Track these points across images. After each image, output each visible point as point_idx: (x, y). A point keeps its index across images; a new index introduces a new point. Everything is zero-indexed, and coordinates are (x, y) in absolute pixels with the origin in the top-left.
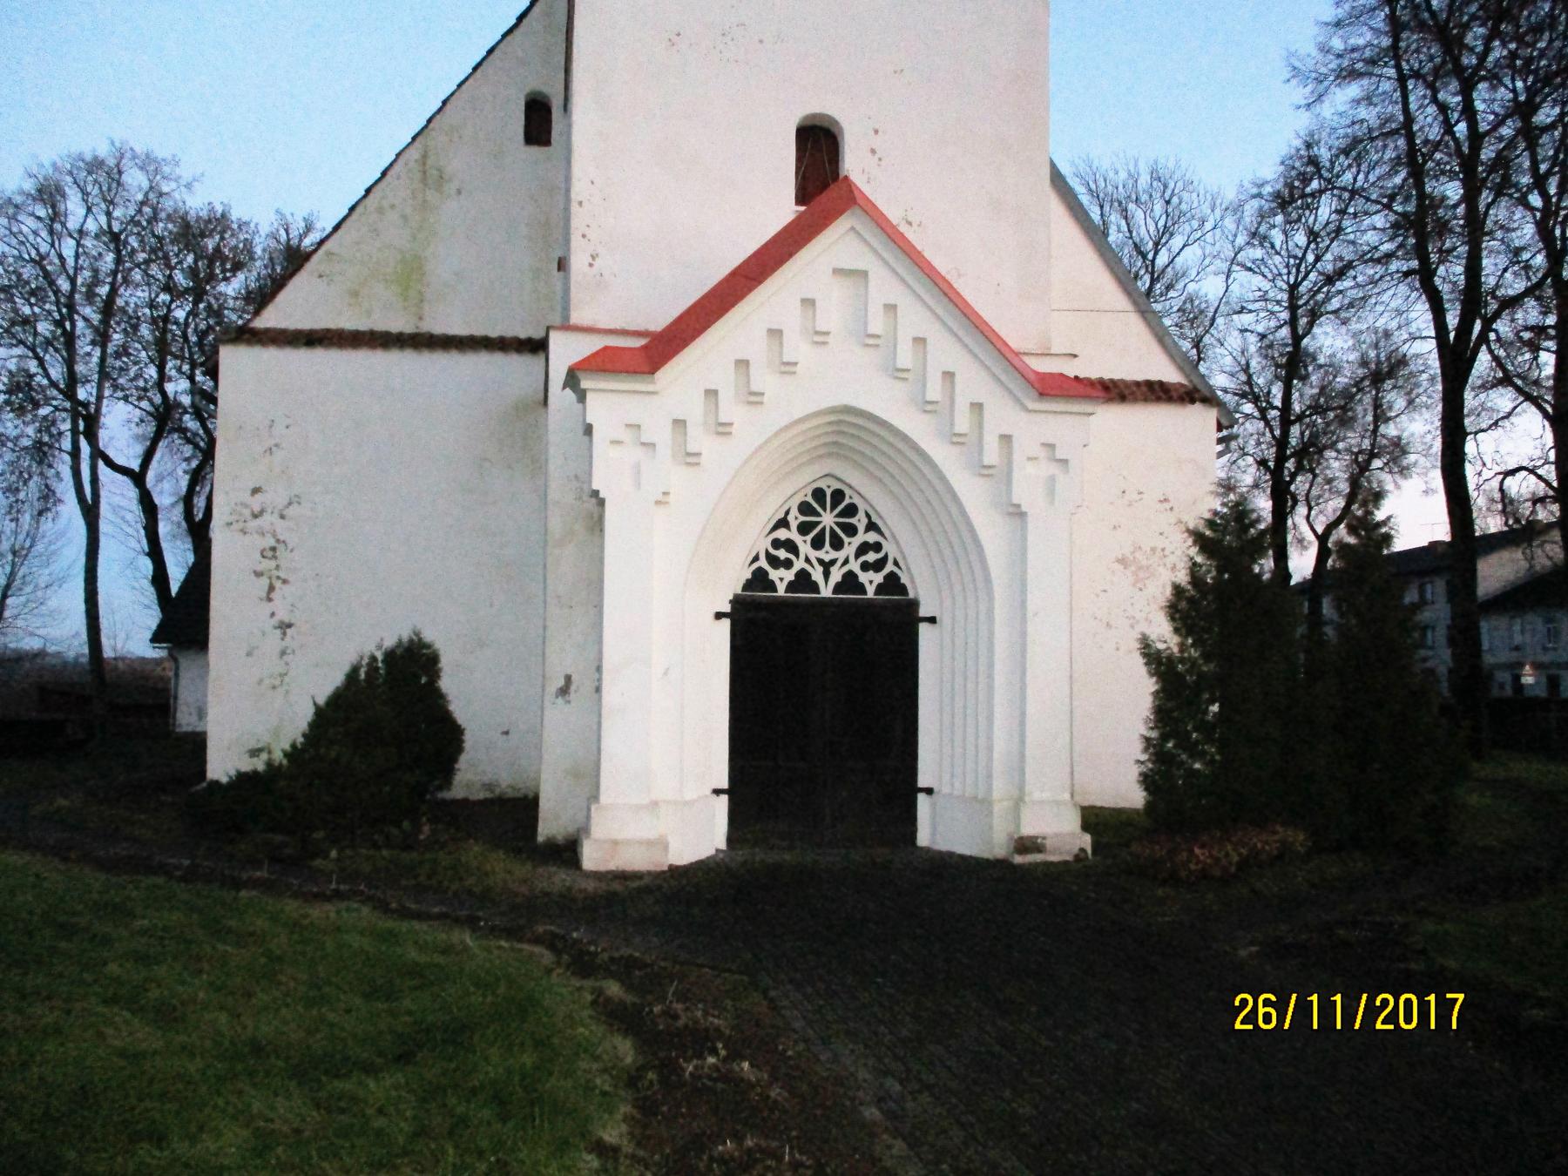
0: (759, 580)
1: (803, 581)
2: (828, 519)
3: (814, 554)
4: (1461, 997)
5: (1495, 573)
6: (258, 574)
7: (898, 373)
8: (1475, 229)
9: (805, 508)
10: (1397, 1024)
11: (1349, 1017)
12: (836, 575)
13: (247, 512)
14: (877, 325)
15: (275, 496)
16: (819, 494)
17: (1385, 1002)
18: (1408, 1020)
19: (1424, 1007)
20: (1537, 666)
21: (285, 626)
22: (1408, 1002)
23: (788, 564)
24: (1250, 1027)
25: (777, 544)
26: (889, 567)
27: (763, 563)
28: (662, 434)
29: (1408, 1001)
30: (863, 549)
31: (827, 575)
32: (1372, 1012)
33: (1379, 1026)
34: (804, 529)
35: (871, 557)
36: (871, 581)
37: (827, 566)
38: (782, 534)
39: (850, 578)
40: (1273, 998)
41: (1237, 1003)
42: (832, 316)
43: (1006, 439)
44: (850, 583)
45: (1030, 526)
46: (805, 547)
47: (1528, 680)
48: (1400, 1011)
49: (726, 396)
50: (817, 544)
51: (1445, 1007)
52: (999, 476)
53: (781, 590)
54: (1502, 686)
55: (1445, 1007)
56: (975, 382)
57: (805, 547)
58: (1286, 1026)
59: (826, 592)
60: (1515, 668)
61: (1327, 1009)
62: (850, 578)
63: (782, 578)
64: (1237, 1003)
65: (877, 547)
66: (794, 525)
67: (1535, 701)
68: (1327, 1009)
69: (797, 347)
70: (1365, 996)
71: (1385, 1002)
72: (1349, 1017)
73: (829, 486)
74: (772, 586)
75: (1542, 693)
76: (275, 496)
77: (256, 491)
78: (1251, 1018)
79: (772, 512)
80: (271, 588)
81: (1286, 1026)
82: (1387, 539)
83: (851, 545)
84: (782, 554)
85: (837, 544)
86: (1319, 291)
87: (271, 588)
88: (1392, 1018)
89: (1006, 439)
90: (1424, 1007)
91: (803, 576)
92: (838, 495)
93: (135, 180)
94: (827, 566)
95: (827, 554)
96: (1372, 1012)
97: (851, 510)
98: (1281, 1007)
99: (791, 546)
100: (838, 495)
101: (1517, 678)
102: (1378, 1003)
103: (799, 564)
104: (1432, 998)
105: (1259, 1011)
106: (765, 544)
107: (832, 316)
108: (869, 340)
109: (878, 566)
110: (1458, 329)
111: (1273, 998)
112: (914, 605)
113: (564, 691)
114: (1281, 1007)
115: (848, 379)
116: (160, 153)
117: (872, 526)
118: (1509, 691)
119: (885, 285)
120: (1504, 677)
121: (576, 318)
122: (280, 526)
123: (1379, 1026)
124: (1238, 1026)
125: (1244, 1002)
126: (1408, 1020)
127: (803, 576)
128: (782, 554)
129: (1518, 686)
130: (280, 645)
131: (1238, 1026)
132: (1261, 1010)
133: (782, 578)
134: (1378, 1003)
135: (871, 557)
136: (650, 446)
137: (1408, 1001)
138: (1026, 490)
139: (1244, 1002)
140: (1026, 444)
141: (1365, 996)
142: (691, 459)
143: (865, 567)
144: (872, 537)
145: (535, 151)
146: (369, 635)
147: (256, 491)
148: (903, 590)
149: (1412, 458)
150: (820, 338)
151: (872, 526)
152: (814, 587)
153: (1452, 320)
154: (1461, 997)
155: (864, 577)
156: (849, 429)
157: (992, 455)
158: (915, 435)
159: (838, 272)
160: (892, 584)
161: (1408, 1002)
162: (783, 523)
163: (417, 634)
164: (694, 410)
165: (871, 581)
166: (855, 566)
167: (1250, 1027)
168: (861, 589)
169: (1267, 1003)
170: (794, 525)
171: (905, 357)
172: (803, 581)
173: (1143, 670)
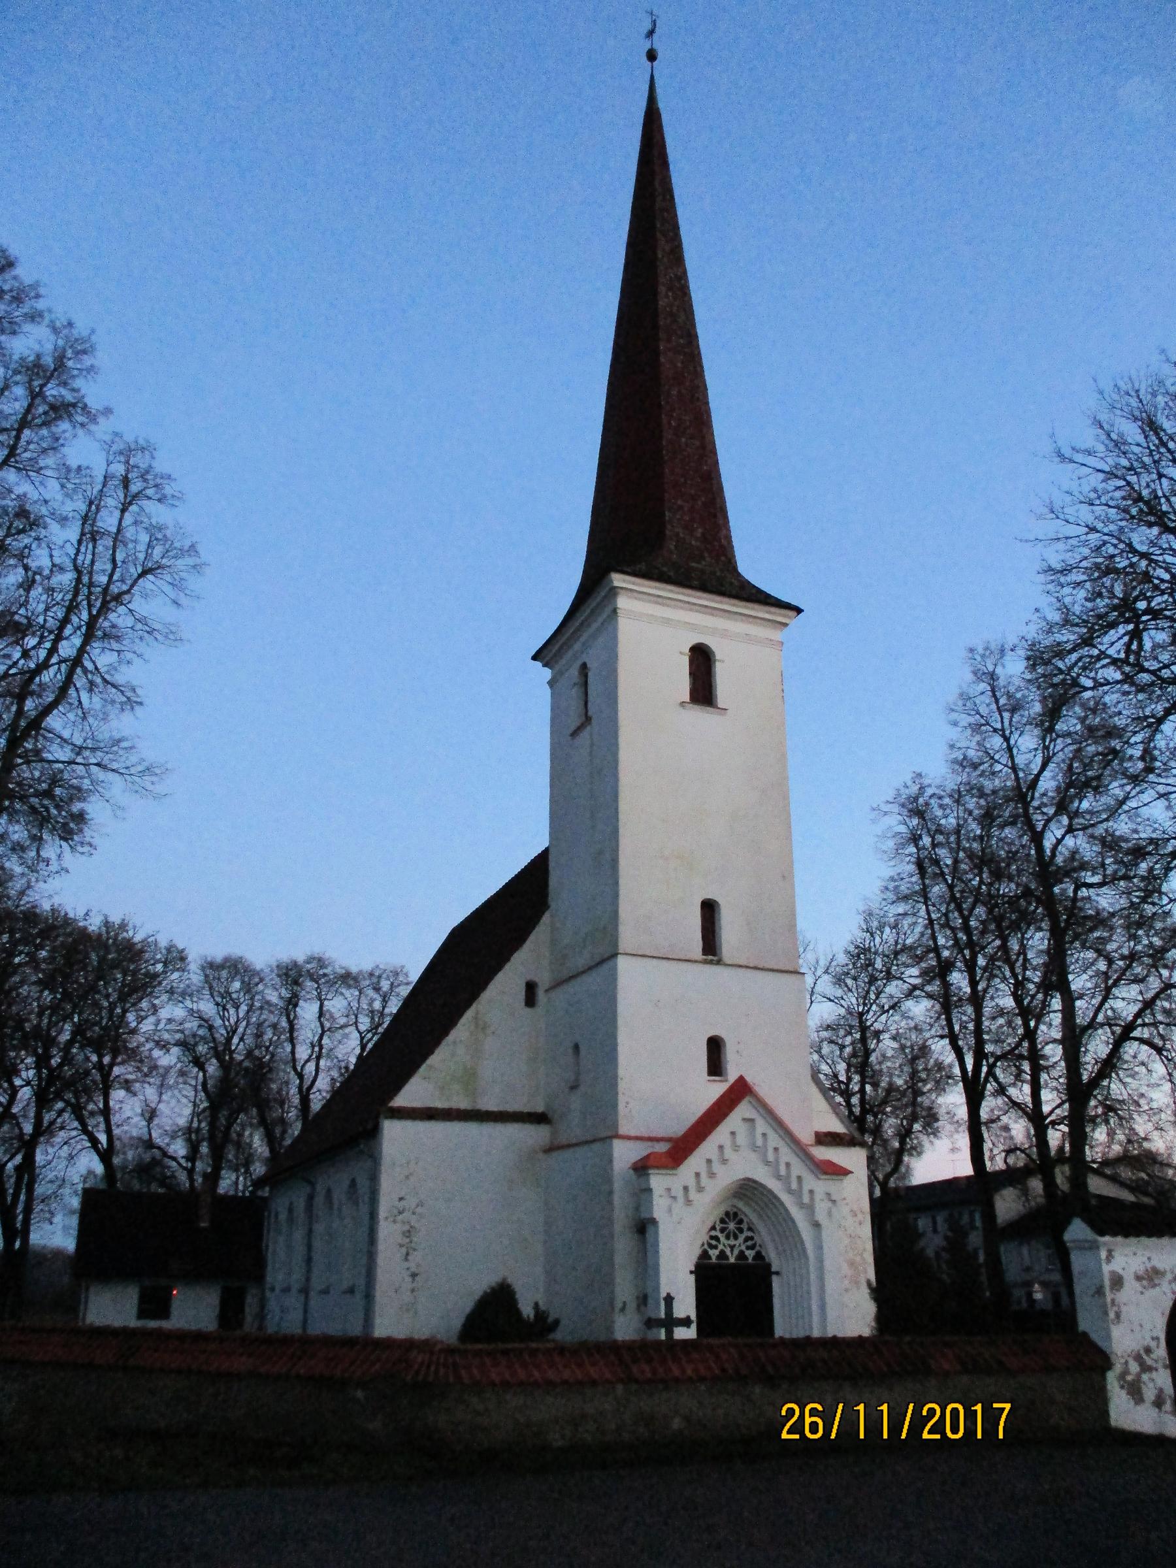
0: (704, 1255)
1: (722, 1255)
2: (732, 1226)
3: (726, 1242)
4: (1008, 1406)
5: (1007, 1205)
6: (401, 1246)
7: (767, 1163)
8: (977, 1000)
9: (722, 1221)
10: (943, 1434)
12: (736, 1252)
13: (396, 1212)
15: (411, 1202)
16: (727, 1214)
17: (932, 1412)
18: (955, 1430)
19: (971, 1416)
20: (1045, 1285)
21: (414, 1275)
22: (955, 1412)
23: (716, 1247)
24: (797, 1437)
25: (712, 1238)
26: (758, 1248)
27: (706, 1246)
28: (680, 1194)
30: (747, 1239)
31: (732, 1251)
34: (722, 1230)
35: (749, 1243)
36: (750, 1254)
38: (713, 1233)
39: (742, 1252)
40: (820, 1408)
42: (742, 1139)
43: (811, 1192)
45: (824, 1234)
46: (722, 1239)
47: (1038, 1296)
49: (704, 1175)
50: (728, 1238)
51: (991, 1417)
52: (810, 1208)
53: (714, 1260)
54: (1019, 1303)
55: (991, 1417)
57: (722, 1239)
59: (732, 1260)
60: (1028, 1284)
62: (742, 1252)
63: (714, 1253)
65: (752, 1238)
66: (718, 1228)
67: (1043, 1313)
69: (728, 1153)
71: (932, 1412)
73: (732, 1210)
74: (710, 1258)
75: (1049, 1306)
76: (411, 1202)
77: (401, 1199)
78: (798, 1428)
79: (710, 1225)
80: (407, 1254)
83: (742, 1237)
84: (714, 1242)
85: (736, 1238)
86: (868, 992)
87: (407, 1254)
88: (939, 1428)
89: (811, 1192)
90: (971, 1416)
91: (722, 1253)
92: (735, 1214)
94: (732, 1247)
95: (732, 1242)
99: (716, 1238)
100: (735, 1214)
101: (1029, 1295)
103: (721, 1247)
104: (979, 1407)
106: (706, 1238)
107: (742, 1139)
108: (754, 1148)
110: (973, 1070)
111: (820, 1408)
112: (769, 1265)
113: (623, 1309)
115: (746, 1165)
117: (750, 1229)
118: (1025, 1305)
119: (761, 1126)
120: (1018, 1293)
121: (622, 1130)
122: (414, 1220)
125: (791, 1412)
126: (955, 1430)
127: (722, 1253)
128: (714, 1242)
129: (1031, 1302)
130: (410, 1286)
133: (714, 1253)
135: (749, 1243)
136: (674, 1198)
138: (821, 1216)
139: (791, 1412)
140: (819, 1196)
142: (688, 1202)
143: (748, 1248)
144: (750, 1234)
145: (528, 1010)
146: (480, 1283)
147: (401, 1199)
148: (763, 1258)
149: (940, 1123)
150: (736, 1148)
152: (727, 1258)
153: (970, 1067)
154: (1008, 1406)
155: (747, 1253)
156: (748, 1190)
157: (806, 1199)
158: (776, 1191)
159: (744, 1119)
160: (759, 1256)
161: (955, 1412)
162: (713, 1228)
163: (504, 1279)
164: (691, 1183)
165: (750, 1254)
166: (743, 1248)
167: (797, 1437)
168: (746, 1258)
169: (814, 1412)
170: (718, 1228)
171: (771, 1157)
172: (722, 1255)
173: (867, 1296)
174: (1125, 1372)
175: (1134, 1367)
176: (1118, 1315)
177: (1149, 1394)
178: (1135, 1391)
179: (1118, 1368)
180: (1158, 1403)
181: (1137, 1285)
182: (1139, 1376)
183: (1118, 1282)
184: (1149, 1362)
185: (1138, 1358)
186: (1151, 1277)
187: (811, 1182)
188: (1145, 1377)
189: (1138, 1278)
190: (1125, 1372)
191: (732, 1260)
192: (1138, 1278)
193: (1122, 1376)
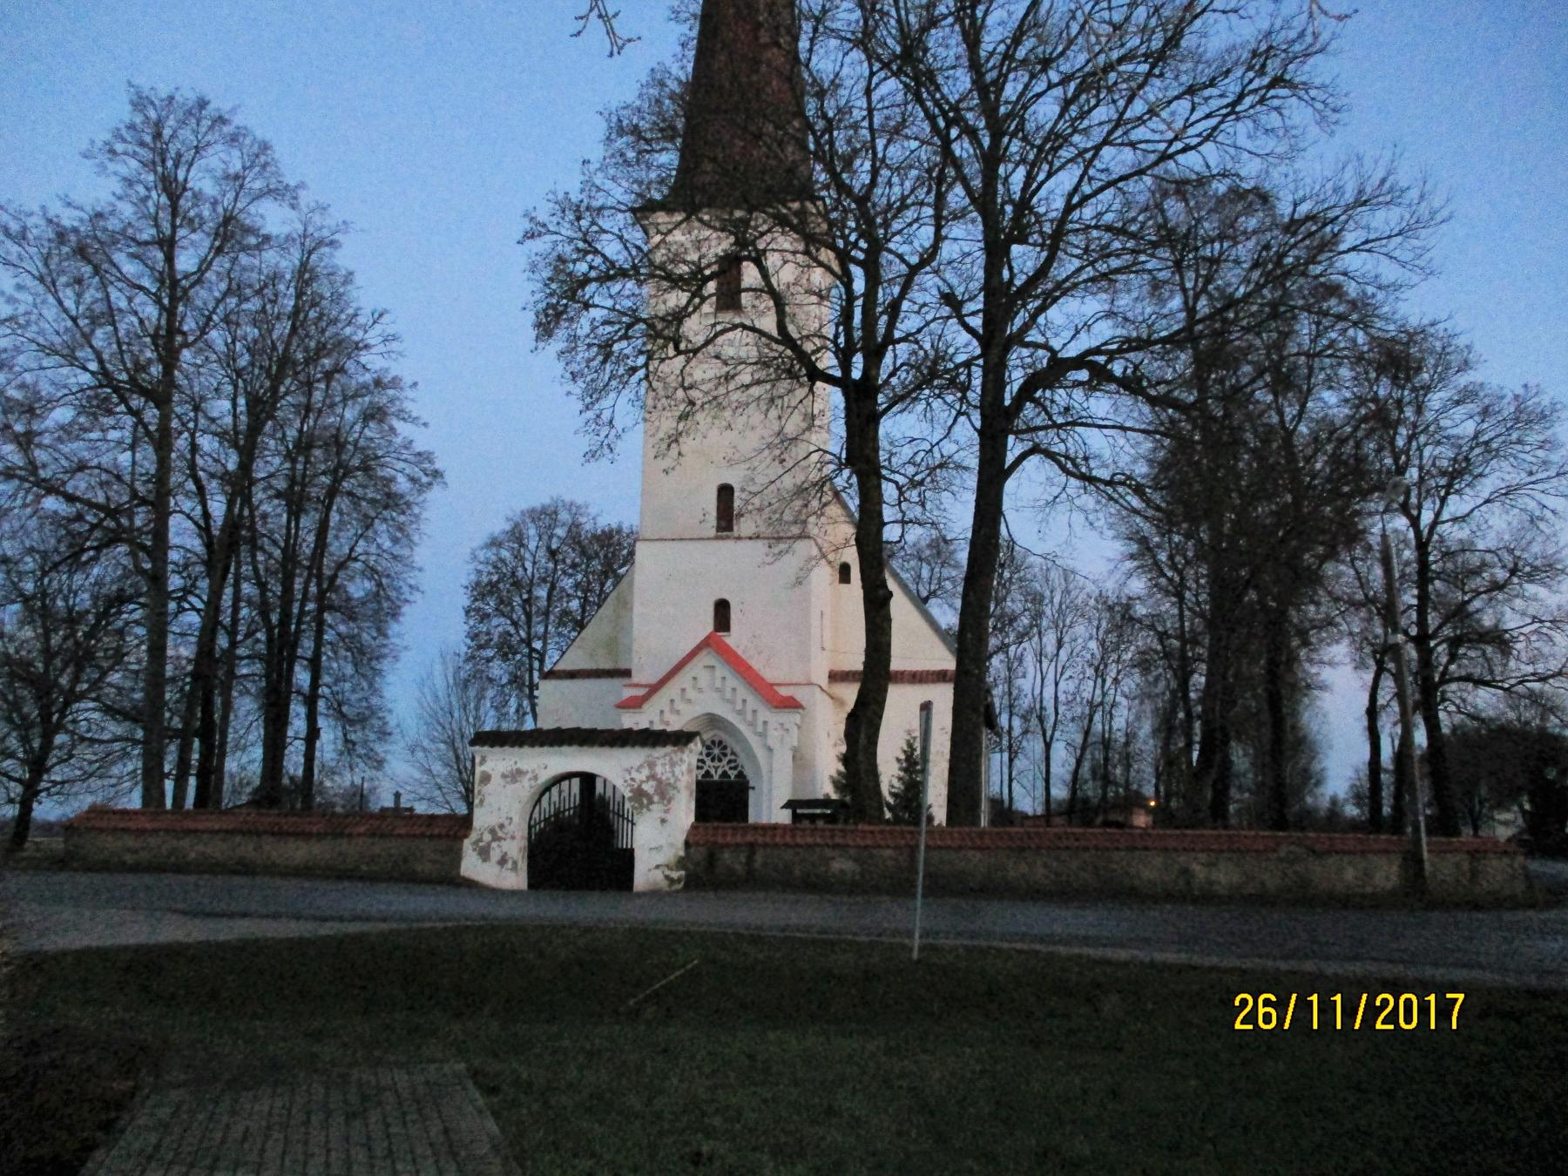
4: (1461, 997)
10: (1397, 1023)
11: (1350, 1013)
12: (720, 771)
14: (718, 684)
17: (1385, 1002)
18: (1408, 1020)
19: (1424, 1009)
22: (1408, 1003)
24: (1250, 1027)
29: (1408, 1001)
32: (1373, 1011)
33: (1379, 1026)
34: (708, 755)
36: (733, 774)
37: (716, 768)
40: (1273, 998)
41: (1237, 1003)
43: (765, 723)
44: (725, 774)
48: (1401, 1012)
51: (1445, 1009)
55: (1445, 1009)
56: (753, 702)
57: (708, 762)
58: (1286, 1026)
59: (716, 778)
61: (1327, 1009)
64: (1237, 1003)
68: (1327, 1009)
70: (1365, 996)
71: (1385, 1002)
72: (1350, 1013)
78: (1251, 1018)
81: (1286, 1026)
82: (839, 773)
88: (1392, 1018)
89: (765, 723)
90: (1424, 1009)
93: (564, 516)
94: (716, 768)
95: (716, 763)
96: (1373, 1011)
97: (725, 748)
98: (1281, 1006)
102: (1378, 1003)
104: (1432, 998)
105: (1259, 1011)
109: (735, 768)
111: (1273, 998)
114: (1281, 1006)
116: (579, 501)
119: (722, 670)
123: (1379, 1026)
124: (1238, 1026)
125: (1244, 1002)
126: (1408, 1020)
131: (1238, 1026)
132: (1261, 1010)
134: (1378, 1003)
137: (1408, 1001)
139: (1244, 1002)
141: (1365, 996)
151: (733, 753)
154: (1461, 997)
160: (741, 775)
161: (1408, 1003)
165: (733, 774)
167: (1250, 1027)
169: (1267, 1003)
174: (480, 840)
175: (487, 837)
176: (482, 801)
177: (495, 855)
178: (484, 853)
179: (474, 836)
180: (503, 861)
181: (502, 782)
182: (489, 844)
183: (486, 778)
184: (500, 834)
185: (492, 831)
186: (515, 776)
187: (765, 714)
188: (494, 845)
189: (504, 776)
190: (480, 840)
191: (716, 778)
192: (504, 776)
193: (476, 843)
